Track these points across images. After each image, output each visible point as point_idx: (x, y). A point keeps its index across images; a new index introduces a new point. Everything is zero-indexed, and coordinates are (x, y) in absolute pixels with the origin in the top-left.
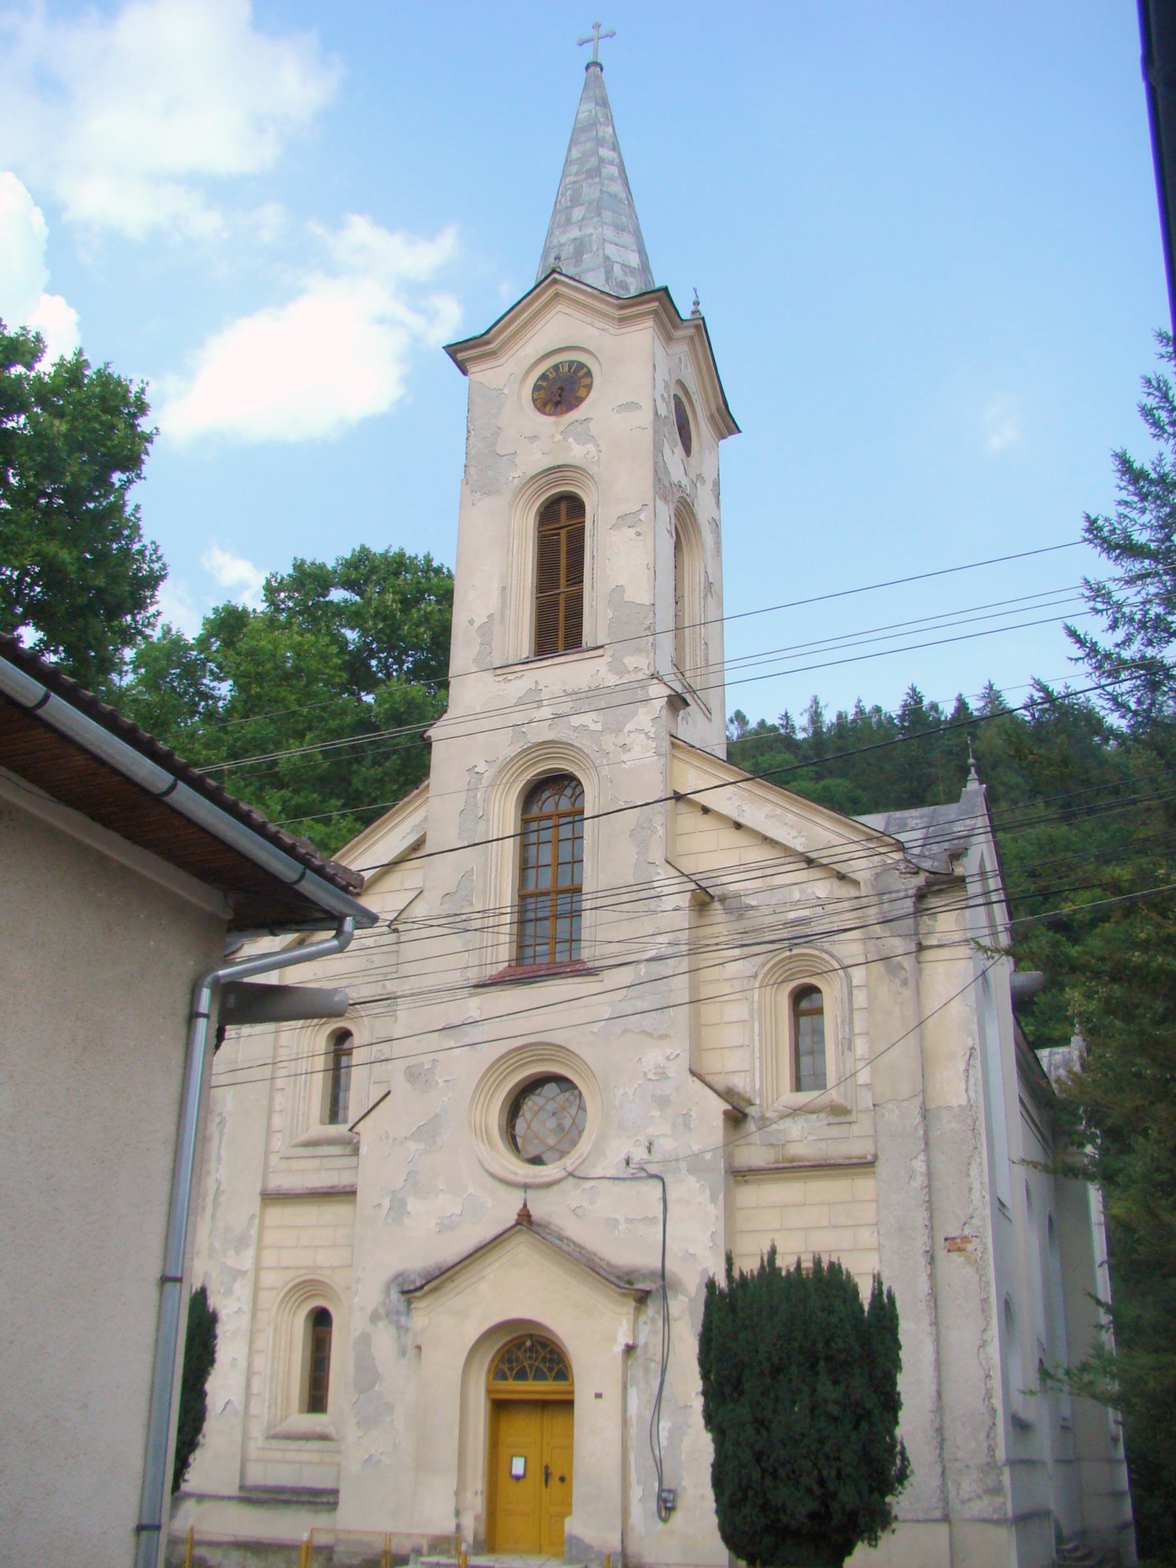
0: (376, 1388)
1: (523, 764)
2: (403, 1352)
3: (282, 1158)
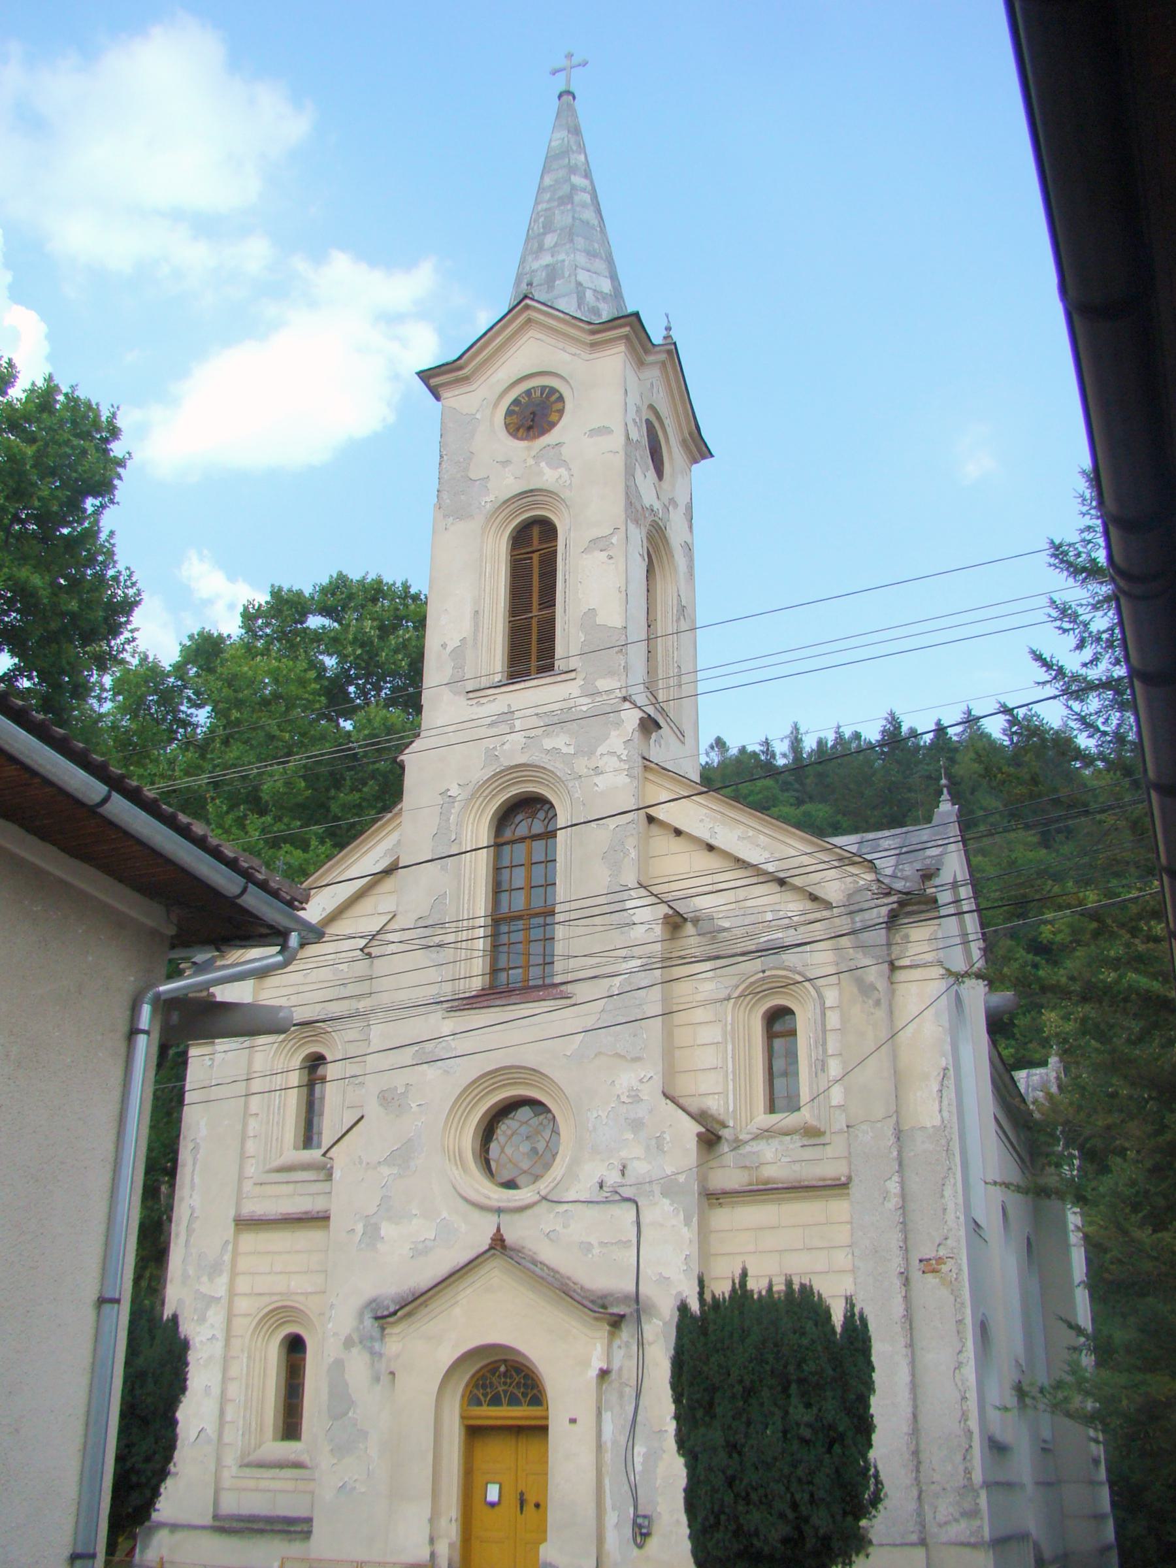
0: (350, 1414)
1: (500, 785)
2: (377, 1379)
3: (255, 1184)
